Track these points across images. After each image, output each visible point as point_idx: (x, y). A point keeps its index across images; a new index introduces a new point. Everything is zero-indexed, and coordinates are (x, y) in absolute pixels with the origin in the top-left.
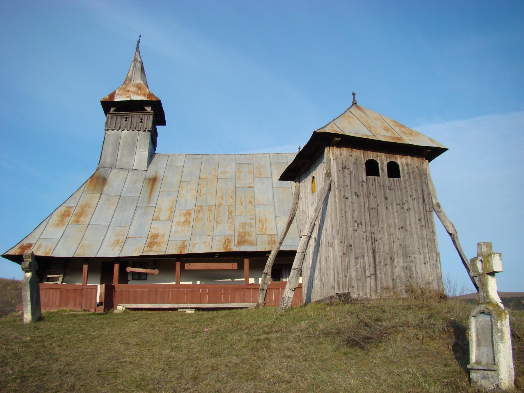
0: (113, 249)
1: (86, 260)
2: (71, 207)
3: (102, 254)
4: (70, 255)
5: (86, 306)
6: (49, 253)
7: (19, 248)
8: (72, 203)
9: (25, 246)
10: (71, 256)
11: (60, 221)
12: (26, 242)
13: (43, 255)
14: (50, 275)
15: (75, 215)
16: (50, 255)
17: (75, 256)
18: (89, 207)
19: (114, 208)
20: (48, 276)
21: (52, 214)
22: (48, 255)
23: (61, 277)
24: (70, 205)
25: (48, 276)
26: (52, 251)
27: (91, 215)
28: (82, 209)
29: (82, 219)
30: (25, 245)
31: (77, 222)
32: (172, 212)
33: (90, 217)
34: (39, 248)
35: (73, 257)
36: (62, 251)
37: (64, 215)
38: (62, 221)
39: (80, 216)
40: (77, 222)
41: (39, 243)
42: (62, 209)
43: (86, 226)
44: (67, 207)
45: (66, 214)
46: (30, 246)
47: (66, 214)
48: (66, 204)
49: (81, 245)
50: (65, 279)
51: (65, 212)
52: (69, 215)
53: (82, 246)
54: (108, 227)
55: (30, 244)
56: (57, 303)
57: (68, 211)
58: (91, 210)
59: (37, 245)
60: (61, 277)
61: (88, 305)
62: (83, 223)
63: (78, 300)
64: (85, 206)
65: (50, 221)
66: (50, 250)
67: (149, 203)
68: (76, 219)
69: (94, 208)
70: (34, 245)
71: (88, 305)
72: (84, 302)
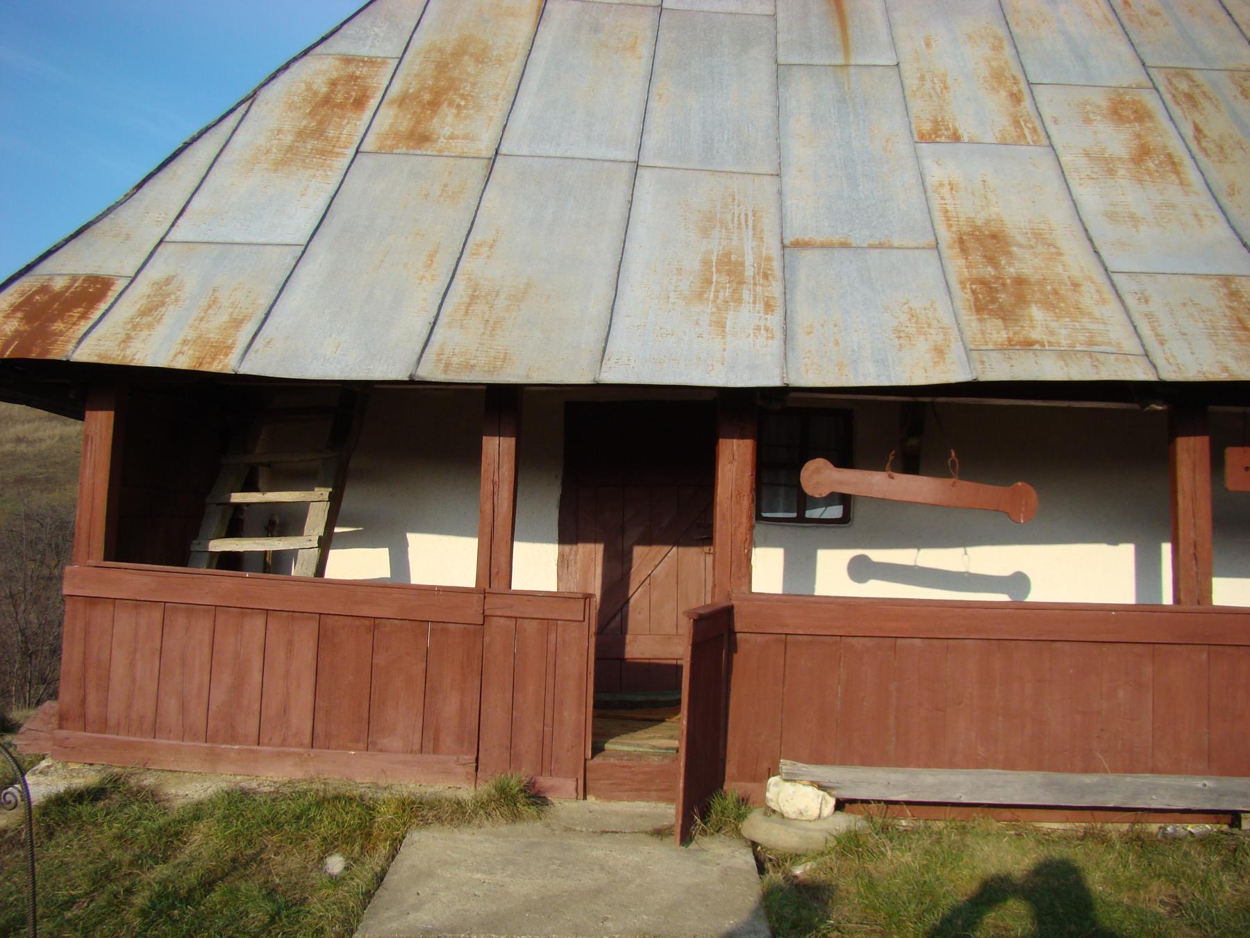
0: (720, 325)
1: (503, 404)
2: (371, 62)
3: (632, 365)
4: (388, 367)
5: (513, 759)
6: (223, 348)
7: (16, 308)
8: (374, 40)
9: (57, 296)
10: (404, 376)
11: (301, 134)
12: (63, 271)
13: (182, 363)
14: (251, 487)
15: (402, 101)
16: (229, 364)
17: (430, 372)
18: (481, 58)
19: (637, 66)
20: (237, 498)
21: (253, 96)
22: (215, 367)
23: (317, 501)
24: (364, 51)
25: (237, 498)
26: (249, 328)
27: (503, 105)
28: (441, 68)
29: (445, 123)
30: (59, 284)
31: (419, 138)
32: (1016, 98)
33: (496, 111)
34: (151, 310)
35: (411, 382)
36: (318, 343)
37: (327, 100)
38: (319, 132)
39: (434, 105)
40: (419, 138)
41: (156, 271)
42: (316, 72)
43: (479, 168)
44: (348, 60)
45: (347, 95)
46: (92, 292)
47: (347, 95)
48: (339, 45)
49: (460, 286)
50: (345, 505)
51: (333, 84)
52: (359, 103)
53: (473, 298)
54: (626, 171)
55: (93, 279)
56: (300, 719)
57: (353, 78)
58: (498, 80)
59: (142, 287)
60: (317, 501)
61: (527, 743)
62: (459, 146)
63: (450, 706)
64: (460, 52)
65: (239, 138)
66: (237, 323)
67: (846, 47)
68: (405, 125)
69: (516, 66)
70: (119, 285)
71: (527, 743)
72: (496, 717)
